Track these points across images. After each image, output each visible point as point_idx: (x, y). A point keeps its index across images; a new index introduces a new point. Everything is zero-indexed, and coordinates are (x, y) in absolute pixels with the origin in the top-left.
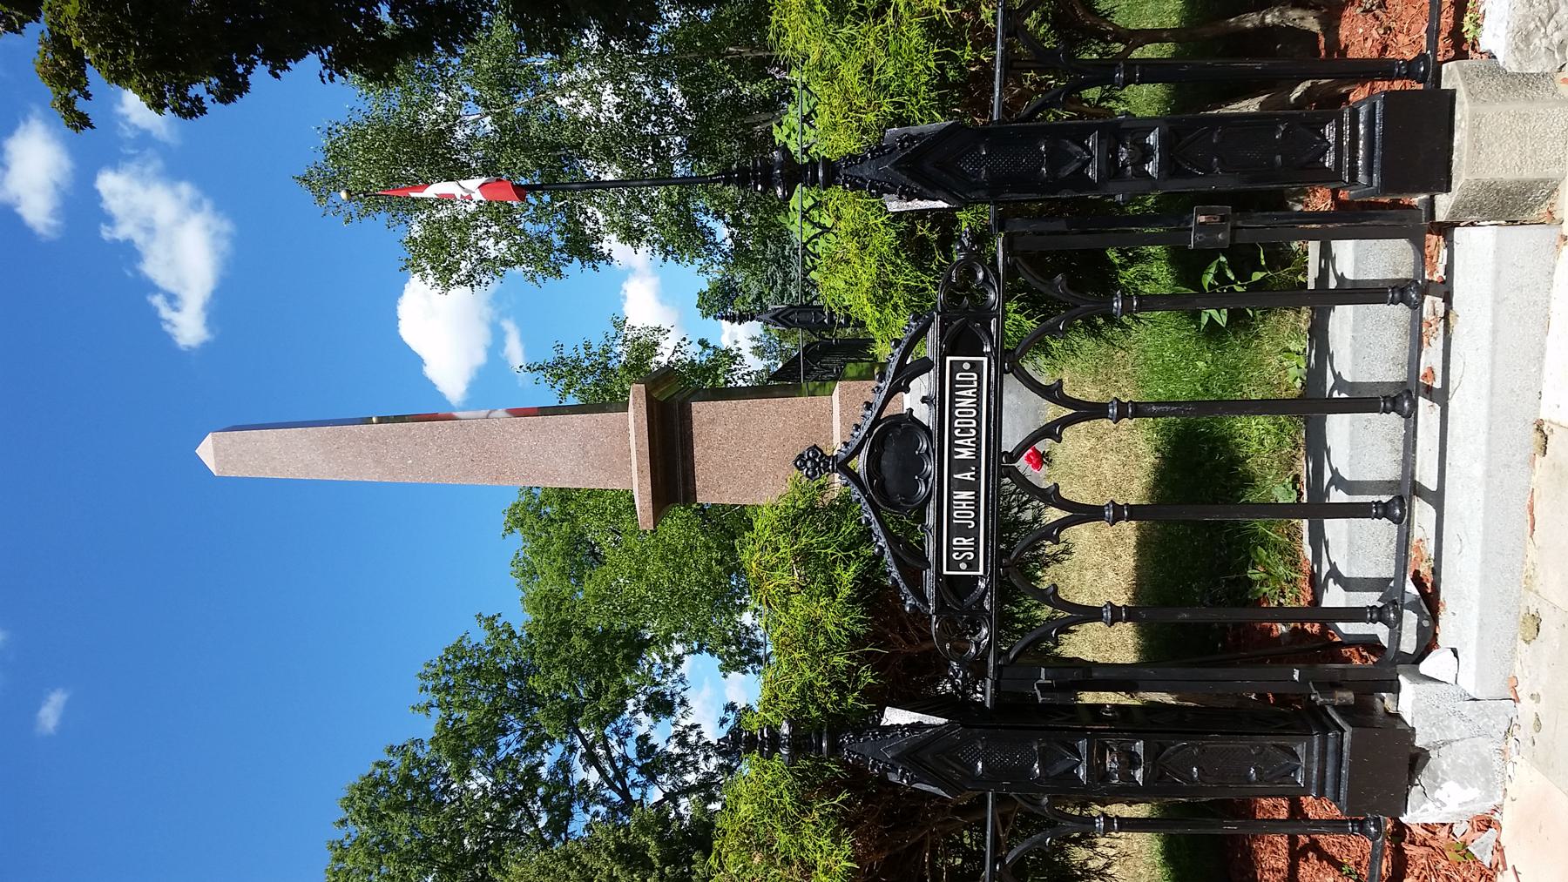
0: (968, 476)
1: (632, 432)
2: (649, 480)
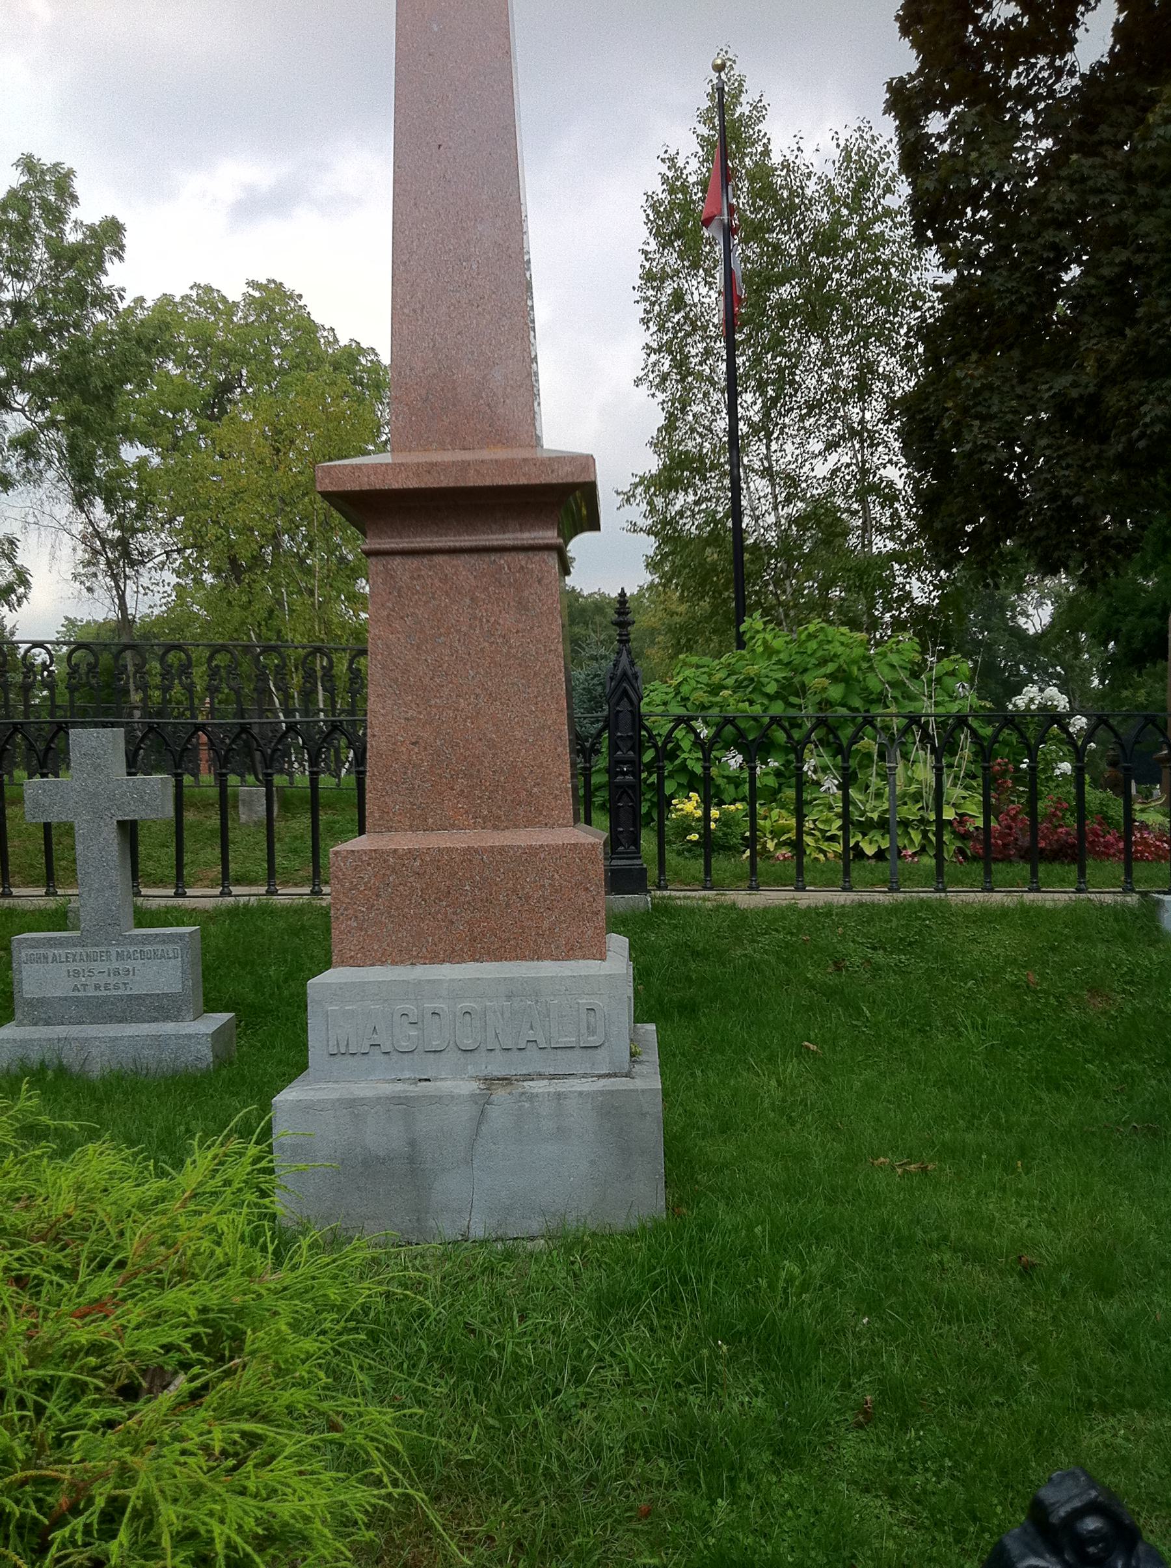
2: (413, 484)
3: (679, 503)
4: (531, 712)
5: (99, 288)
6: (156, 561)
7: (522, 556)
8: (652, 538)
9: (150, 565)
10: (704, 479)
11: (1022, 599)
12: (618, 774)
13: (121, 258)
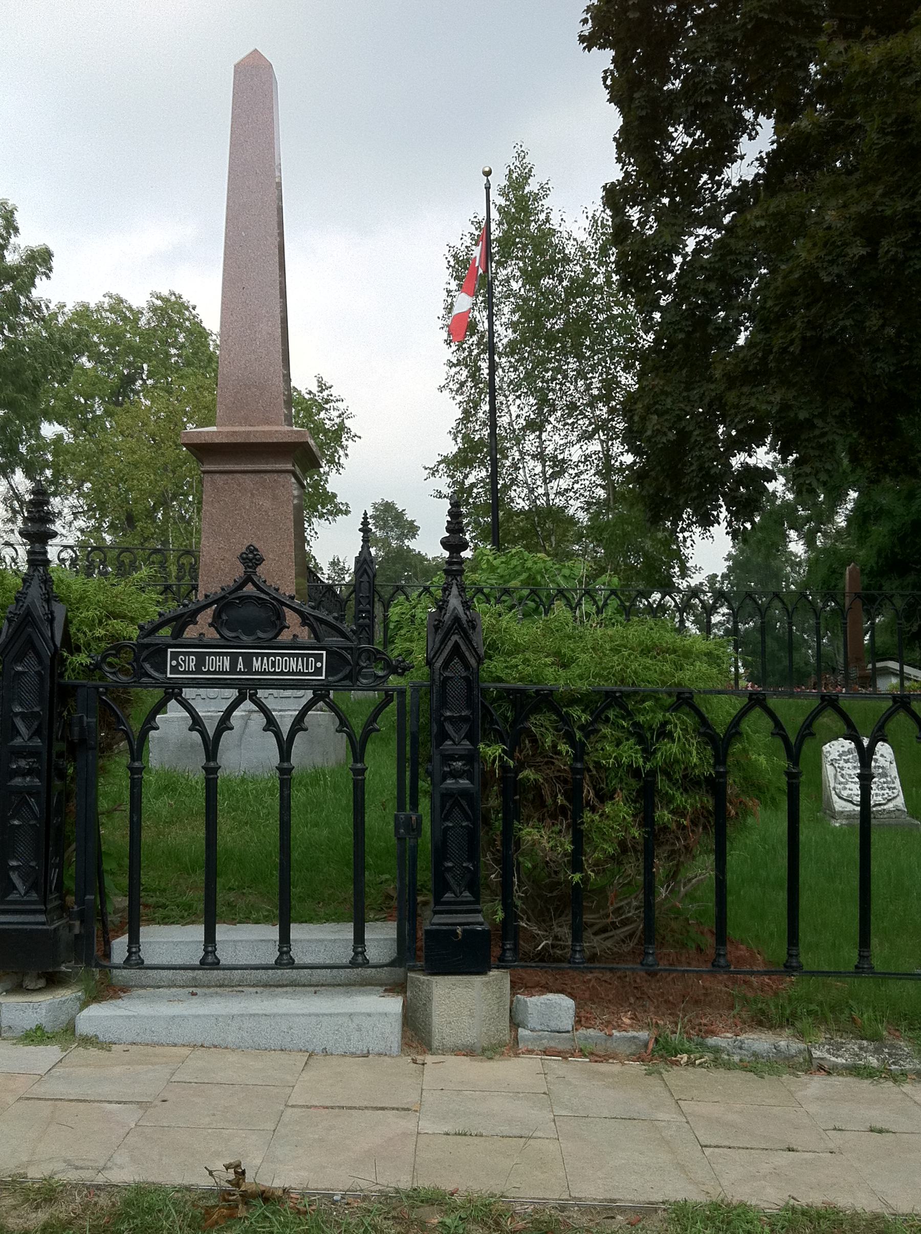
0: (240, 666)
1: (267, 428)
2: (225, 440)
5: (30, 300)
12: (359, 618)
13: (48, 277)
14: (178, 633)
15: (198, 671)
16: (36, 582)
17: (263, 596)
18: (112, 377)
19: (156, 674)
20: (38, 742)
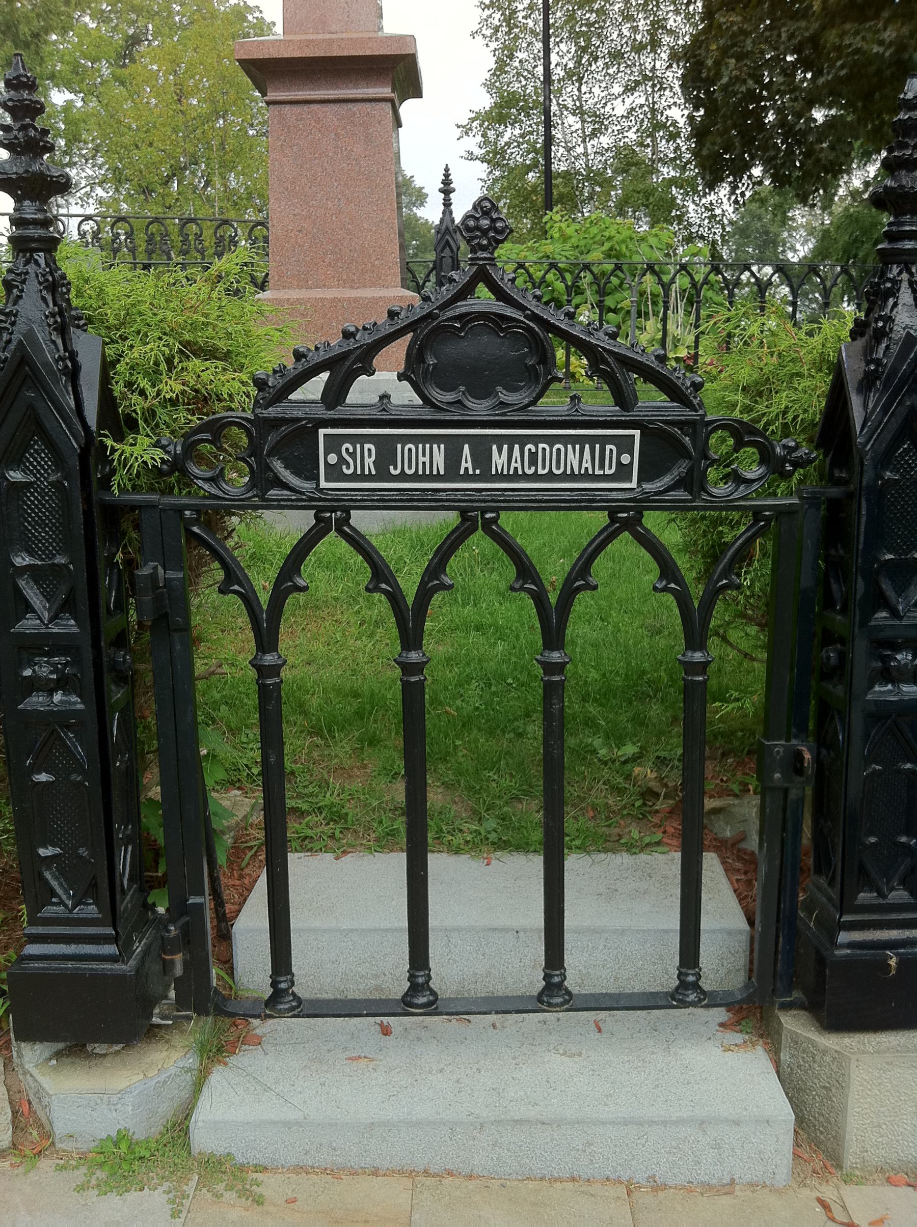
0: (467, 464)
2: (297, 54)
3: (507, 135)
4: (374, 211)
6: (83, 191)
7: (368, 105)
8: (485, 164)
9: (78, 194)
10: (528, 115)
11: (791, 236)
14: (335, 394)
15: (382, 474)
16: (32, 287)
17: (509, 312)
18: (116, 37)
19: (294, 481)
20: (69, 625)
